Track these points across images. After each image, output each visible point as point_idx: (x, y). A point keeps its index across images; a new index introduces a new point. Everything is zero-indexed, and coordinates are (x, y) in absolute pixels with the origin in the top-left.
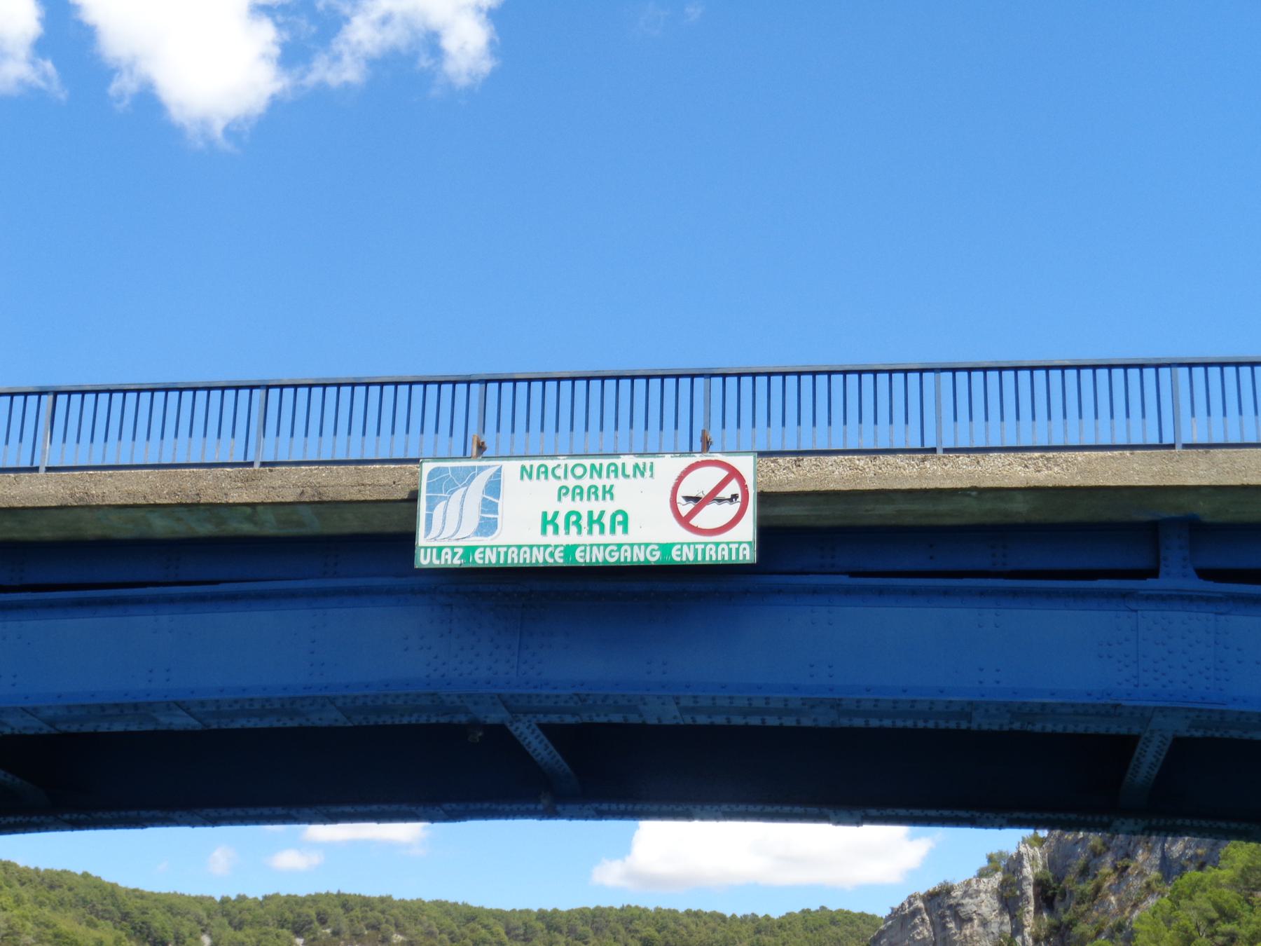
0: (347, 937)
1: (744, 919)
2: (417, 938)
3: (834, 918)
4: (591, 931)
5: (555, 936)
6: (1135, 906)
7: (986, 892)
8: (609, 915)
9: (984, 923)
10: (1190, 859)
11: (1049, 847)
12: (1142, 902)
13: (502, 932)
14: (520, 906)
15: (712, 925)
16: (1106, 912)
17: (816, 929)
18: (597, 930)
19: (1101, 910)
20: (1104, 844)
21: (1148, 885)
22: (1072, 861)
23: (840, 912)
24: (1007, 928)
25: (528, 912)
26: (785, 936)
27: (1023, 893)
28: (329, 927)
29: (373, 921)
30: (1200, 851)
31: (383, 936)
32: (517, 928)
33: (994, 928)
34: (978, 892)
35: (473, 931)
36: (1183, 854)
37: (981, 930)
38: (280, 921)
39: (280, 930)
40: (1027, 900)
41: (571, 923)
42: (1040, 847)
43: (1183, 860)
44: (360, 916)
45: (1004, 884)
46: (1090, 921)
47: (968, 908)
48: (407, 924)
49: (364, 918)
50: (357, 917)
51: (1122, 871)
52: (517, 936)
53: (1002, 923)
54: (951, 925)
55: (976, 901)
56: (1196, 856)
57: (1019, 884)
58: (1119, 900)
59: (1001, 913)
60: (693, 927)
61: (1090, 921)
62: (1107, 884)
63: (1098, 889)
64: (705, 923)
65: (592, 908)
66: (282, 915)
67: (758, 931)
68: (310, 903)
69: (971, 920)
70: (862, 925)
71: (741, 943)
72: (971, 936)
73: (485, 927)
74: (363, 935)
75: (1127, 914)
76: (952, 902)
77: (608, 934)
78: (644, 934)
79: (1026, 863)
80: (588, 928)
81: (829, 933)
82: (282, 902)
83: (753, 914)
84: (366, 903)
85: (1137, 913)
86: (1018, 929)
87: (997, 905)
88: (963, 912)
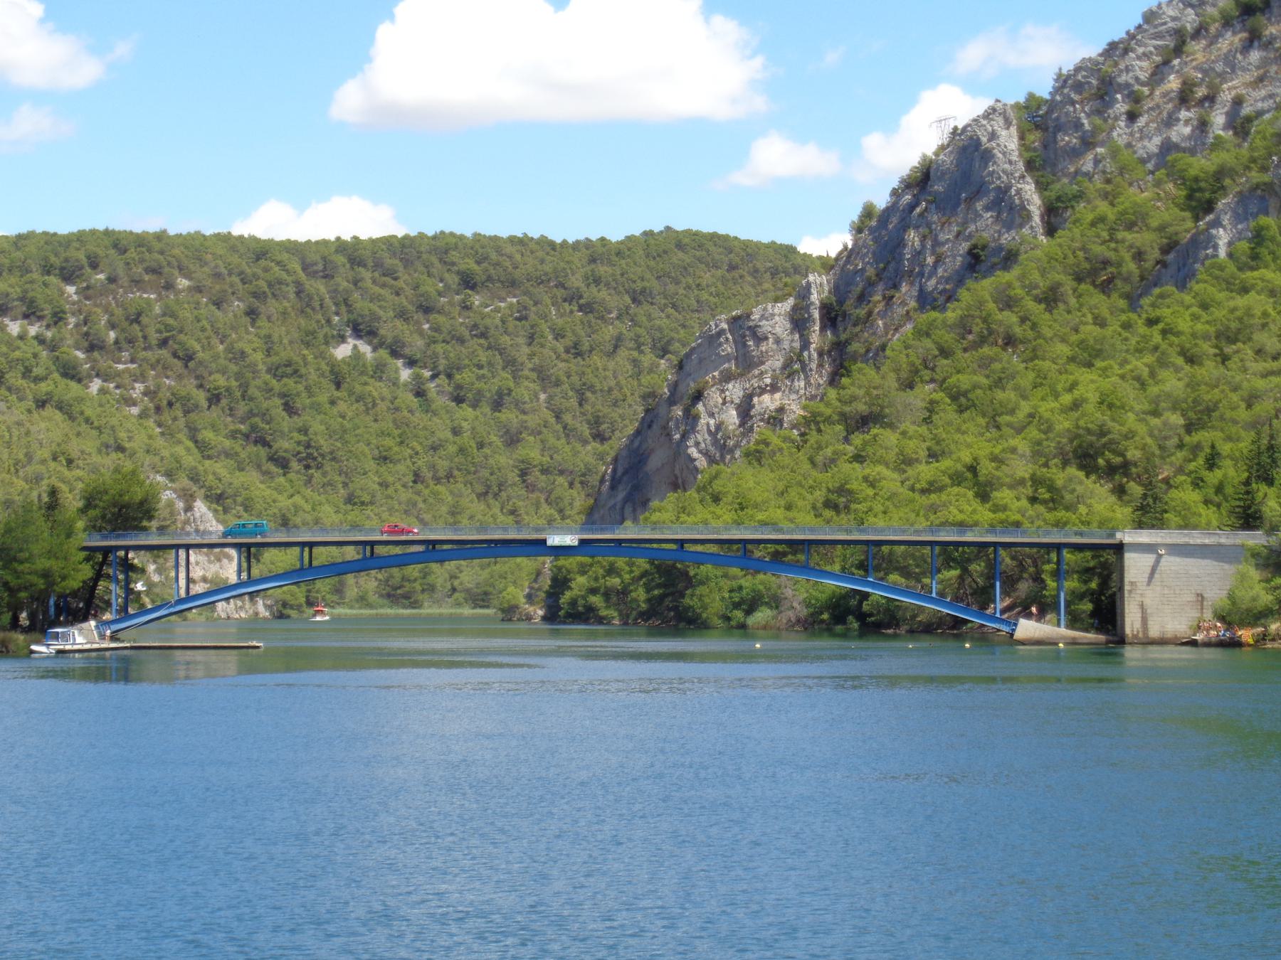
0: (126, 284)
1: (577, 244)
2: (204, 283)
3: (680, 241)
4: (400, 264)
5: (359, 273)
6: (896, 330)
7: (780, 315)
8: (420, 245)
9: (778, 341)
10: (940, 293)
11: (835, 274)
12: (901, 326)
13: (298, 268)
14: (315, 236)
15: (540, 254)
16: (874, 334)
17: (659, 256)
18: (407, 263)
19: (871, 331)
20: (877, 275)
21: (908, 312)
22: (853, 288)
23: (688, 232)
24: (797, 345)
25: (325, 243)
26: (624, 266)
27: (810, 316)
28: (102, 272)
29: (154, 264)
30: (948, 287)
31: (167, 282)
32: (316, 264)
33: (786, 345)
34: (773, 315)
35: (266, 270)
36: (936, 288)
37: (775, 347)
38: (45, 266)
39: (47, 278)
40: (814, 321)
41: (377, 255)
42: (828, 273)
43: (935, 295)
44: (137, 258)
45: (795, 308)
46: (862, 340)
47: (764, 329)
48: (191, 266)
49: (142, 261)
50: (134, 259)
51: (888, 300)
52: (316, 272)
53: (792, 341)
54: (751, 343)
55: (771, 323)
56: (944, 291)
57: (808, 307)
58: (885, 324)
59: (792, 333)
60: (518, 257)
61: (862, 340)
62: (877, 310)
63: (870, 314)
64: (532, 252)
65: (400, 236)
66: (46, 259)
67: (593, 260)
68: (76, 245)
69: (766, 338)
70: (712, 248)
71: (573, 275)
72: (767, 352)
73: (278, 263)
74: (144, 281)
75: (889, 336)
76: (751, 324)
77: (421, 268)
78: (463, 267)
79: (814, 291)
80: (397, 262)
81: (675, 260)
82: (42, 242)
83: (587, 239)
84: (141, 241)
85: (897, 336)
86: (805, 345)
87: (788, 326)
88: (760, 332)
